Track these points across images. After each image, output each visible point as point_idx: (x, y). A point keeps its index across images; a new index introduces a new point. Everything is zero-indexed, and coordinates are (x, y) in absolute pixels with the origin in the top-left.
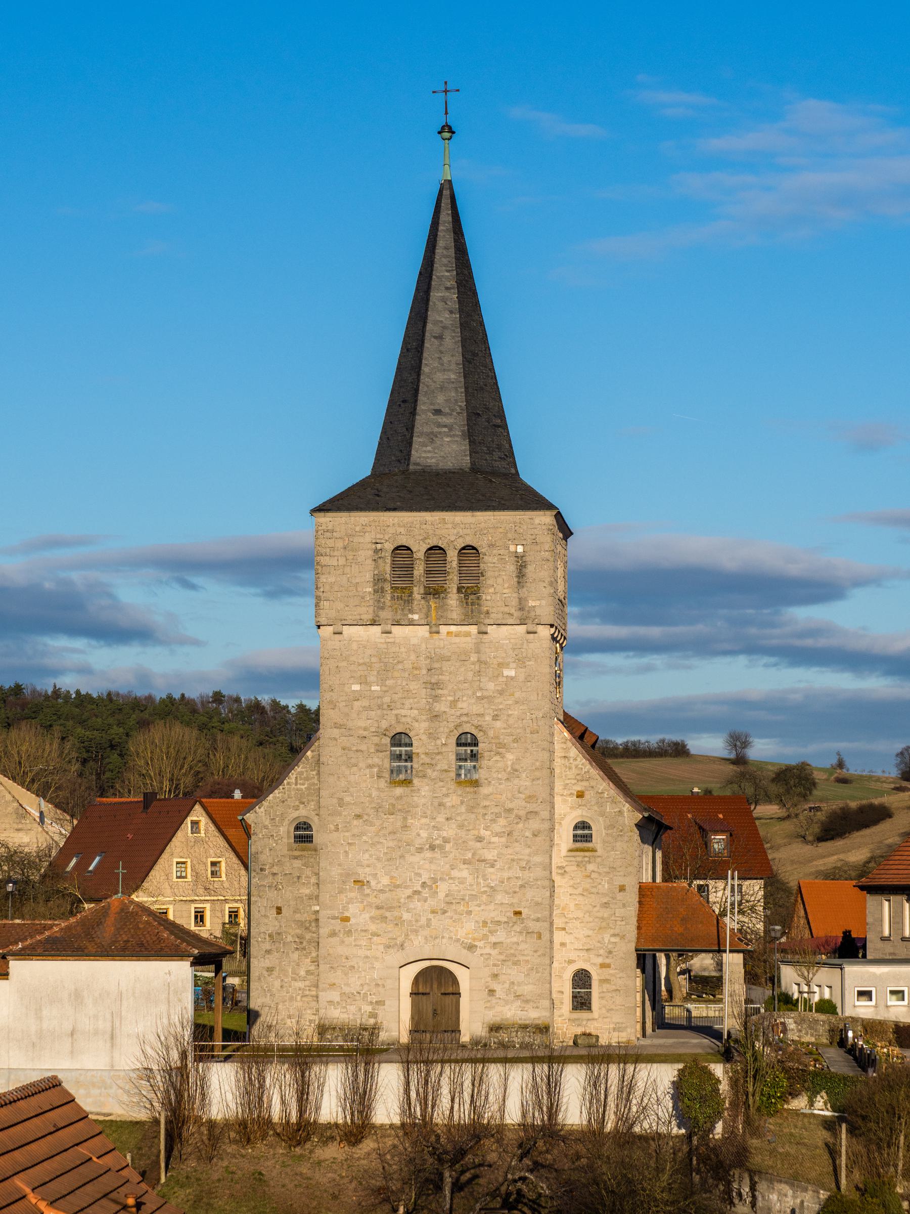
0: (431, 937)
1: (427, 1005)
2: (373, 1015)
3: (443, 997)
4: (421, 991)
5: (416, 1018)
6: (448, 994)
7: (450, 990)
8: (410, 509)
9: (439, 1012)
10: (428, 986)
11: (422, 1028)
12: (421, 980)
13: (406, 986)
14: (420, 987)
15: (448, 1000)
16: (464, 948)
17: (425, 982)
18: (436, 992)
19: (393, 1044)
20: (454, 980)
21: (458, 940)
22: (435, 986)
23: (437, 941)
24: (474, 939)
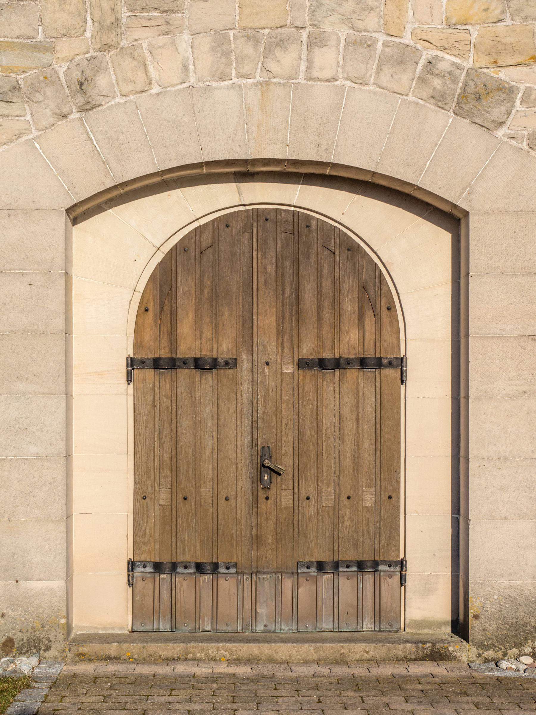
0: (251, 35)
1: (222, 424)
2: (61, 553)
3: (308, 378)
4: (188, 345)
5: (163, 497)
6: (337, 364)
7: (351, 342)
8: (355, 241)
9: (286, 462)
10: (229, 318)
11: (192, 550)
12: (186, 286)
13: (106, 318)
14: (185, 327)
15: (343, 396)
16: (440, 100)
17: (213, 300)
18: (268, 364)
19: (34, 646)
20: (375, 295)
21: (402, 57)
22: (267, 320)
23: (286, 60)
24: (496, 53)
